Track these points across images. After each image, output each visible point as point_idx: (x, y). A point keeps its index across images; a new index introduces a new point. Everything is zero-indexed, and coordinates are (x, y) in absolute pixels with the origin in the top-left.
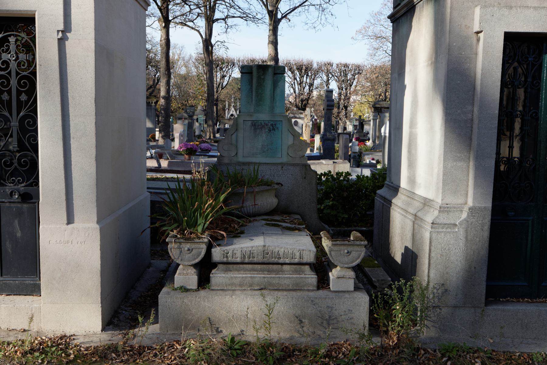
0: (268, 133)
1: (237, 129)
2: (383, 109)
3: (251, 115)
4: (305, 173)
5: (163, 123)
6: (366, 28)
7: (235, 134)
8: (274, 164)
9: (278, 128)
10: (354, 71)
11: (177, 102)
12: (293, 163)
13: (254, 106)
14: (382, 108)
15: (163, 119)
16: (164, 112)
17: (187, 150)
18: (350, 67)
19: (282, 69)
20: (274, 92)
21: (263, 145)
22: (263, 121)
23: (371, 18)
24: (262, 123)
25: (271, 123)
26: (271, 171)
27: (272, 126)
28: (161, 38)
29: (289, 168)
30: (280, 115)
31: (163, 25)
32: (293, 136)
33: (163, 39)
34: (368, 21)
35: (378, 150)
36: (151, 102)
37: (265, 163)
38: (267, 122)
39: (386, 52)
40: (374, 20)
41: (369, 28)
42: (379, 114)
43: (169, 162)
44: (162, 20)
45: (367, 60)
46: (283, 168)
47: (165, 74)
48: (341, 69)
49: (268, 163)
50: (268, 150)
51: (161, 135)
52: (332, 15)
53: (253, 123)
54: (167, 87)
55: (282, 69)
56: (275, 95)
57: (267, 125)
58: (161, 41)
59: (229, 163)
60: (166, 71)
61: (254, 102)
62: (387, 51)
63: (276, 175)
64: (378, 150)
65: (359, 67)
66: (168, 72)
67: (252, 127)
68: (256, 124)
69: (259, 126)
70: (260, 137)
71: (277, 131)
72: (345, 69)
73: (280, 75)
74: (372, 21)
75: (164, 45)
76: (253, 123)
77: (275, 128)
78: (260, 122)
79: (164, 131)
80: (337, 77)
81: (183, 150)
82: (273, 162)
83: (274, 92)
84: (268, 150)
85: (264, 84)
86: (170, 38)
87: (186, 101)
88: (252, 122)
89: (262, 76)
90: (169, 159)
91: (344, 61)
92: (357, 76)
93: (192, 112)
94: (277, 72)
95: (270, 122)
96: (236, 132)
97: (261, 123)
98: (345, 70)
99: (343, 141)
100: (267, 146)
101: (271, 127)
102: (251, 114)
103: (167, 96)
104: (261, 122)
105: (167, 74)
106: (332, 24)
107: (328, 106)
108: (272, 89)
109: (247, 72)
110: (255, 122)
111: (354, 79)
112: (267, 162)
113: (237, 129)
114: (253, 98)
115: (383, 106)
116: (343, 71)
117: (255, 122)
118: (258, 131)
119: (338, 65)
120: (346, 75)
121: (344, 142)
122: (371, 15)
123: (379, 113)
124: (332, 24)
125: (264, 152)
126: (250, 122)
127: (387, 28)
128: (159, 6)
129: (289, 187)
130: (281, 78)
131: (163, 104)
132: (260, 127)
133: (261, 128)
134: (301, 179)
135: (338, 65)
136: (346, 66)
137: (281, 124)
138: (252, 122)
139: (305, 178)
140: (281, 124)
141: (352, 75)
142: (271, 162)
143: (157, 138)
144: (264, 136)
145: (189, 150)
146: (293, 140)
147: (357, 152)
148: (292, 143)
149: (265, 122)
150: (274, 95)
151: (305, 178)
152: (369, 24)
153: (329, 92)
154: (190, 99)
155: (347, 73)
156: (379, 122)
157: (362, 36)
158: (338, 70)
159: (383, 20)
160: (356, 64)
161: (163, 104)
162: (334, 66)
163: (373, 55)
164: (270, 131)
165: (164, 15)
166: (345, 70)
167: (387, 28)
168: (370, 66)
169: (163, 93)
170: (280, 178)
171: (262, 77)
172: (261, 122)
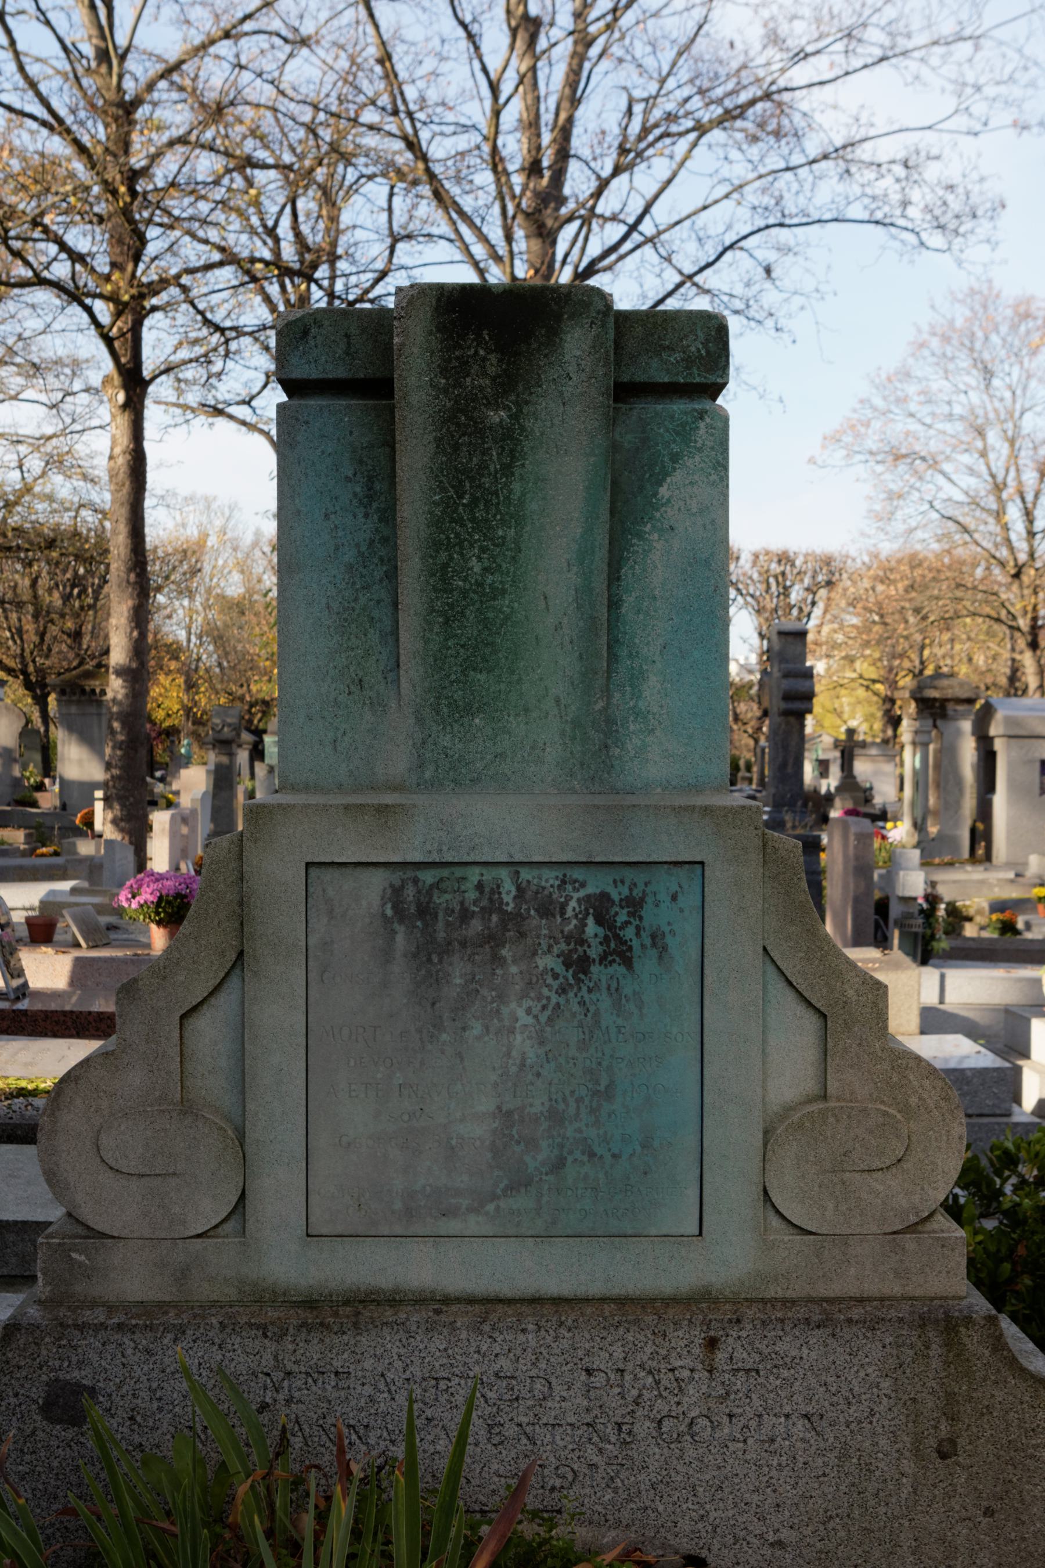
0: (563, 991)
1: (241, 954)
2: (950, 706)
3: (382, 810)
4: (950, 1396)
5: (120, 768)
6: (855, 428)
7: (226, 1002)
8: (622, 1302)
9: (657, 939)
10: (813, 577)
11: (213, 687)
12: (823, 1290)
13: (420, 720)
14: (947, 700)
15: (119, 753)
16: (123, 728)
17: (158, 905)
18: (798, 563)
19: (695, 346)
20: (614, 576)
21: (505, 1115)
22: (504, 873)
23: (874, 391)
24: (497, 889)
25: (590, 890)
26: (599, 1380)
27: (599, 921)
28: (112, 449)
29: (787, 1347)
30: (679, 810)
31: (121, 397)
32: (811, 1022)
33: (118, 450)
34: (862, 401)
35: (937, 861)
36: (98, 691)
37: (535, 1301)
38: (549, 878)
39: (932, 507)
40: (885, 398)
41: (867, 425)
42: (935, 726)
43: (78, 962)
44: (117, 380)
45: (863, 534)
46: (721, 1356)
47: (128, 582)
48: (767, 571)
49: (558, 1301)
50: (559, 1165)
51: (110, 816)
52: (777, 330)
53: (410, 892)
54: (135, 634)
55: (695, 346)
56: (629, 600)
57: (548, 909)
58: (111, 458)
59: (162, 1306)
60: (130, 570)
61: (412, 672)
62: (935, 503)
63: (643, 1428)
64: (937, 861)
65: (828, 564)
66: (138, 575)
67: (400, 929)
68: (440, 899)
69: (465, 915)
70: (477, 1028)
71: (646, 964)
72: (782, 568)
73: (679, 407)
74: (878, 402)
75: (121, 475)
76: (410, 892)
77: (629, 933)
78: (474, 875)
79: (122, 799)
80: (752, 596)
81: (142, 906)
82: (617, 1290)
83: (614, 576)
84: (559, 1165)
85: (516, 487)
86: (147, 445)
87: (242, 686)
88: (396, 878)
89: (494, 404)
90: (78, 945)
91: (776, 545)
92: (823, 593)
93: (229, 725)
94: (641, 377)
95: (577, 874)
96: (234, 981)
97: (489, 893)
98: (783, 574)
99: (845, 845)
100: (556, 1117)
101: (591, 928)
102: (389, 799)
103: (134, 665)
104: (488, 875)
105: (136, 583)
106: (761, 389)
107: (787, 697)
108: (601, 538)
109: (341, 372)
110: (428, 877)
111: (813, 603)
112: (553, 1286)
113: (241, 954)
114: (404, 636)
115: (950, 693)
116: (776, 577)
117: (428, 877)
118: (458, 970)
119: (756, 556)
120: (786, 591)
121: (851, 850)
122: (873, 382)
123: (935, 721)
124: (761, 389)
125: (519, 1183)
126: (377, 882)
127: (930, 426)
128: (103, 327)
129: (780, 1544)
130: (685, 432)
131: (120, 697)
132: (476, 926)
133: (493, 940)
134: (908, 1466)
135: (756, 556)
136: (784, 558)
137: (690, 900)
138: (396, 878)
139: (945, 1452)
140: (690, 900)
141: (807, 589)
142: (596, 1289)
143: (98, 826)
144: (524, 1019)
145: (168, 902)
146: (812, 1055)
147: (915, 899)
148: (810, 1085)
149: (525, 874)
150: (614, 604)
151: (943, 1456)
152: (869, 413)
153: (790, 639)
154: (256, 678)
155: (788, 583)
156: (936, 751)
157: (844, 452)
158: (755, 576)
159: (916, 398)
160: (818, 551)
161: (120, 697)
162: (742, 562)
163: (885, 518)
164: (579, 965)
165: (123, 360)
166: (783, 574)
167: (930, 426)
168: (866, 559)
169: (118, 655)
170: (691, 1453)
171: (497, 417)
172: (488, 875)
